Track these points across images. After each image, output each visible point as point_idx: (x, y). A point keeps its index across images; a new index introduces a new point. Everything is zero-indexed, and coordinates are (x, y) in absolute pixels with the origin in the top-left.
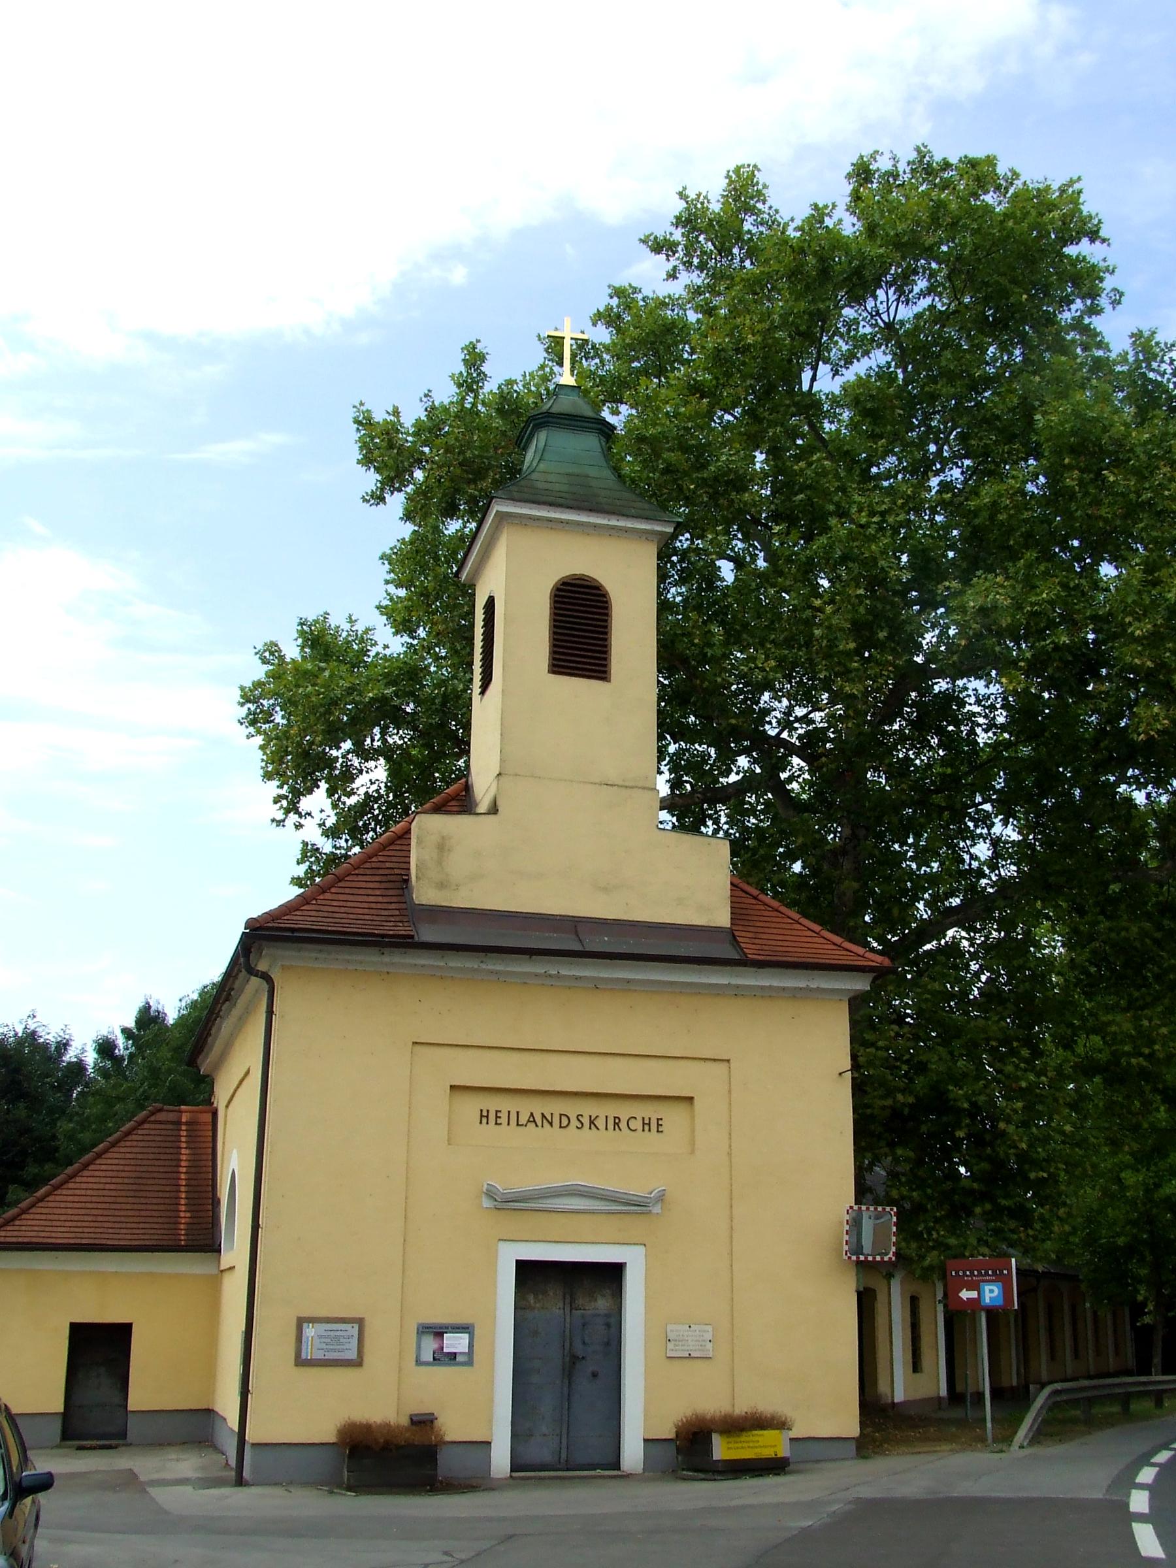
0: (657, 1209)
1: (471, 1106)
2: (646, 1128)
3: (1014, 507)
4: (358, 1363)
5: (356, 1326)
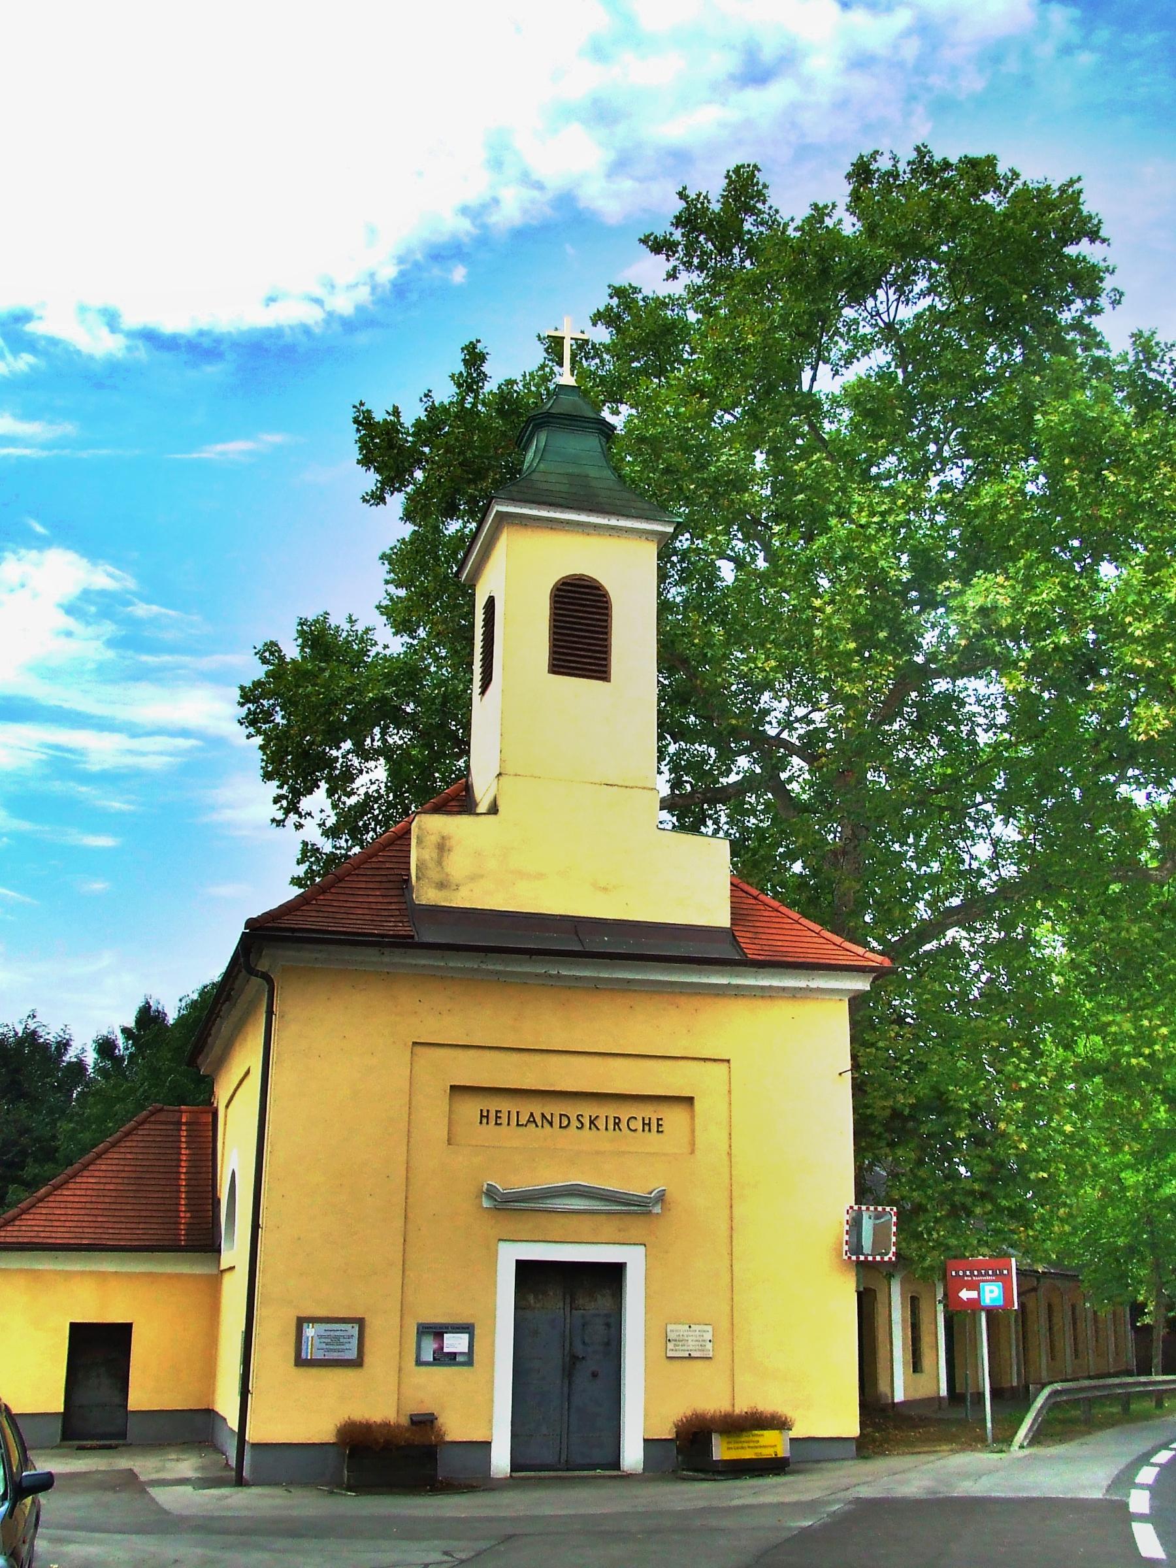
0: (657, 1209)
1: (471, 1108)
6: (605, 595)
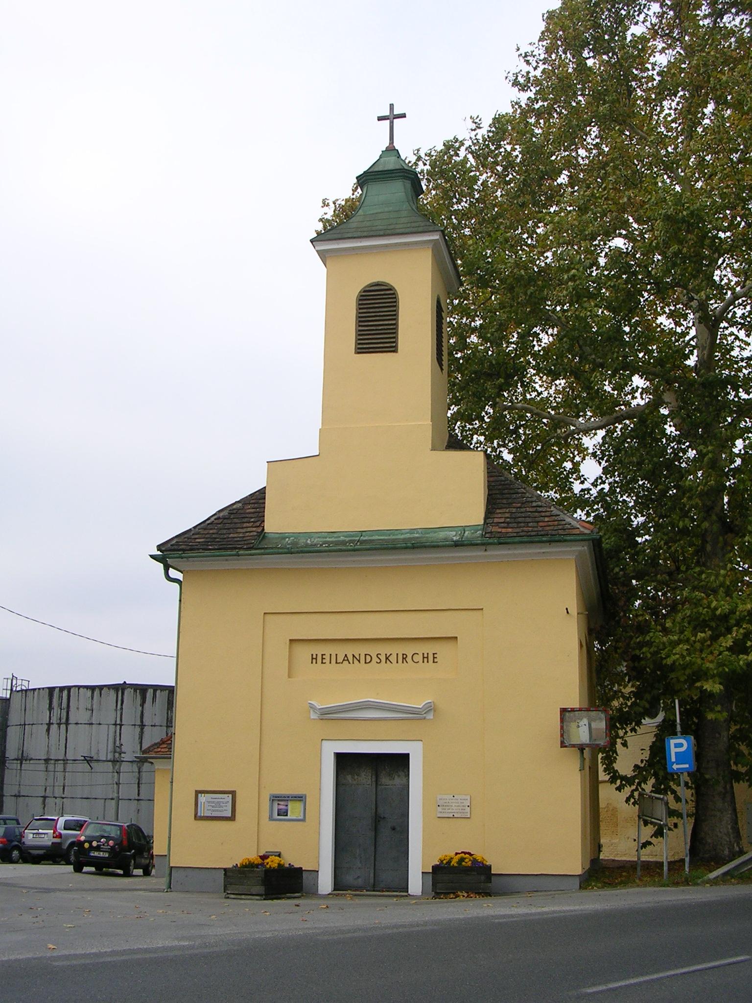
0: (430, 716)
1: (304, 653)
2: (426, 660)
3: (567, 445)
4: (232, 818)
5: (230, 796)
6: (391, 288)
